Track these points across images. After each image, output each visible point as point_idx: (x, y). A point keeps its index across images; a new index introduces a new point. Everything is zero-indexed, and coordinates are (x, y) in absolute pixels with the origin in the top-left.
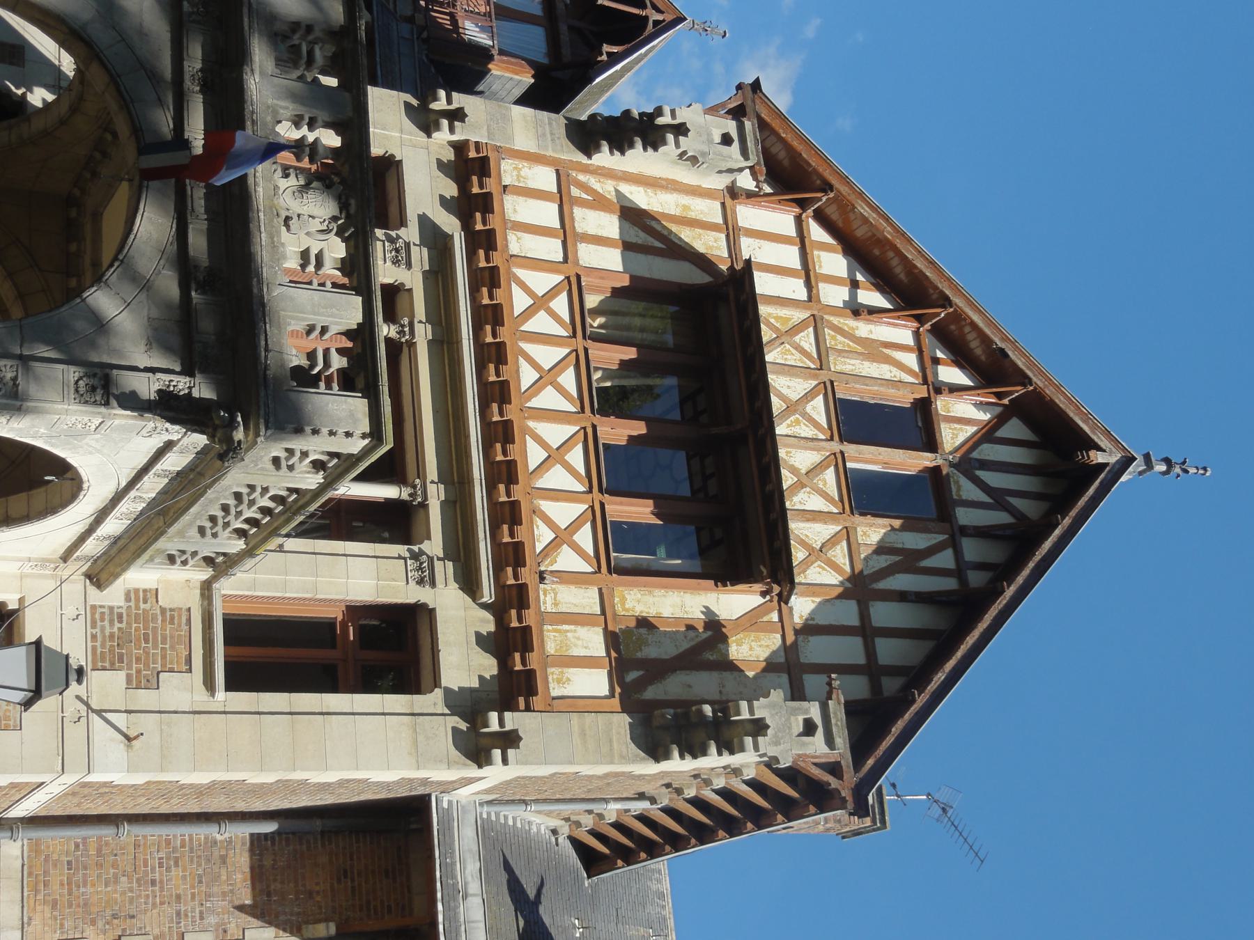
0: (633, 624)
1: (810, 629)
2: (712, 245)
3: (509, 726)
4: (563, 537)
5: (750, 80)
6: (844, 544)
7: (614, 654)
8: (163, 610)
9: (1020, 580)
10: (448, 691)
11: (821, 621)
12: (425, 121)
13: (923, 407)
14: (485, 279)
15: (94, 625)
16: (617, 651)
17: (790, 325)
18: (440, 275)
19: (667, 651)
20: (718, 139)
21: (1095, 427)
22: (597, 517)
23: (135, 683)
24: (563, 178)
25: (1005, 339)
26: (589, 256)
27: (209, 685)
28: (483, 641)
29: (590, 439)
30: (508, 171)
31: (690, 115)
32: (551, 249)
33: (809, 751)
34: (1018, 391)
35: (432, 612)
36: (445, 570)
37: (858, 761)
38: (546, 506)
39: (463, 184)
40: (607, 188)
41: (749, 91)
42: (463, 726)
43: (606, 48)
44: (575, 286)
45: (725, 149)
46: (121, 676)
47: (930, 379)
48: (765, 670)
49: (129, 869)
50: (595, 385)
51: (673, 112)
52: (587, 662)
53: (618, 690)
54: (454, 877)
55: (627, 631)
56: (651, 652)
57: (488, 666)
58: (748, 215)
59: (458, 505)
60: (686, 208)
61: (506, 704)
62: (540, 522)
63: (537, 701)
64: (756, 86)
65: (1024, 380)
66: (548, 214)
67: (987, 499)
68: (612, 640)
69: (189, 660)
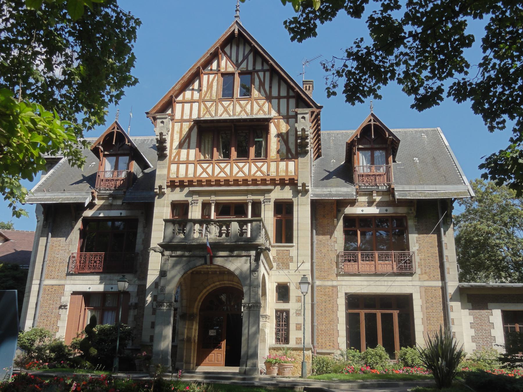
0: (278, 155)
1: (279, 112)
2: (186, 127)
4: (259, 169)
5: (146, 115)
6: (258, 101)
7: (285, 160)
8: (277, 255)
9: (268, 58)
10: (293, 197)
11: (277, 109)
12: (162, 194)
13: (223, 75)
14: (200, 183)
15: (280, 269)
16: (284, 159)
17: (205, 108)
18: (199, 193)
20: (162, 125)
21: (229, 31)
22: (254, 161)
23: (292, 261)
24: (173, 163)
25: (207, 53)
26: (192, 158)
27: (292, 246)
28: (282, 189)
29: (236, 162)
30: (173, 176)
31: (157, 132)
32: (191, 167)
33: (308, 119)
34: (220, 50)
35: (276, 199)
36: (267, 196)
37: (311, 107)
38: (253, 172)
39: (177, 186)
40: (174, 152)
42: (300, 194)
43: (127, 143)
44: (200, 162)
46: (290, 264)
47: (216, 72)
48: (288, 124)
49: (322, 260)
50: (223, 159)
51: (157, 136)
52: (287, 166)
53: (293, 160)
54: (327, 194)
55: (280, 156)
56: (284, 151)
57: (287, 188)
58: (178, 116)
59: (253, 192)
60: (177, 132)
61: (296, 184)
62: (256, 175)
63: (296, 178)
64: (147, 113)
66: (182, 167)
68: (282, 160)
69: (287, 250)
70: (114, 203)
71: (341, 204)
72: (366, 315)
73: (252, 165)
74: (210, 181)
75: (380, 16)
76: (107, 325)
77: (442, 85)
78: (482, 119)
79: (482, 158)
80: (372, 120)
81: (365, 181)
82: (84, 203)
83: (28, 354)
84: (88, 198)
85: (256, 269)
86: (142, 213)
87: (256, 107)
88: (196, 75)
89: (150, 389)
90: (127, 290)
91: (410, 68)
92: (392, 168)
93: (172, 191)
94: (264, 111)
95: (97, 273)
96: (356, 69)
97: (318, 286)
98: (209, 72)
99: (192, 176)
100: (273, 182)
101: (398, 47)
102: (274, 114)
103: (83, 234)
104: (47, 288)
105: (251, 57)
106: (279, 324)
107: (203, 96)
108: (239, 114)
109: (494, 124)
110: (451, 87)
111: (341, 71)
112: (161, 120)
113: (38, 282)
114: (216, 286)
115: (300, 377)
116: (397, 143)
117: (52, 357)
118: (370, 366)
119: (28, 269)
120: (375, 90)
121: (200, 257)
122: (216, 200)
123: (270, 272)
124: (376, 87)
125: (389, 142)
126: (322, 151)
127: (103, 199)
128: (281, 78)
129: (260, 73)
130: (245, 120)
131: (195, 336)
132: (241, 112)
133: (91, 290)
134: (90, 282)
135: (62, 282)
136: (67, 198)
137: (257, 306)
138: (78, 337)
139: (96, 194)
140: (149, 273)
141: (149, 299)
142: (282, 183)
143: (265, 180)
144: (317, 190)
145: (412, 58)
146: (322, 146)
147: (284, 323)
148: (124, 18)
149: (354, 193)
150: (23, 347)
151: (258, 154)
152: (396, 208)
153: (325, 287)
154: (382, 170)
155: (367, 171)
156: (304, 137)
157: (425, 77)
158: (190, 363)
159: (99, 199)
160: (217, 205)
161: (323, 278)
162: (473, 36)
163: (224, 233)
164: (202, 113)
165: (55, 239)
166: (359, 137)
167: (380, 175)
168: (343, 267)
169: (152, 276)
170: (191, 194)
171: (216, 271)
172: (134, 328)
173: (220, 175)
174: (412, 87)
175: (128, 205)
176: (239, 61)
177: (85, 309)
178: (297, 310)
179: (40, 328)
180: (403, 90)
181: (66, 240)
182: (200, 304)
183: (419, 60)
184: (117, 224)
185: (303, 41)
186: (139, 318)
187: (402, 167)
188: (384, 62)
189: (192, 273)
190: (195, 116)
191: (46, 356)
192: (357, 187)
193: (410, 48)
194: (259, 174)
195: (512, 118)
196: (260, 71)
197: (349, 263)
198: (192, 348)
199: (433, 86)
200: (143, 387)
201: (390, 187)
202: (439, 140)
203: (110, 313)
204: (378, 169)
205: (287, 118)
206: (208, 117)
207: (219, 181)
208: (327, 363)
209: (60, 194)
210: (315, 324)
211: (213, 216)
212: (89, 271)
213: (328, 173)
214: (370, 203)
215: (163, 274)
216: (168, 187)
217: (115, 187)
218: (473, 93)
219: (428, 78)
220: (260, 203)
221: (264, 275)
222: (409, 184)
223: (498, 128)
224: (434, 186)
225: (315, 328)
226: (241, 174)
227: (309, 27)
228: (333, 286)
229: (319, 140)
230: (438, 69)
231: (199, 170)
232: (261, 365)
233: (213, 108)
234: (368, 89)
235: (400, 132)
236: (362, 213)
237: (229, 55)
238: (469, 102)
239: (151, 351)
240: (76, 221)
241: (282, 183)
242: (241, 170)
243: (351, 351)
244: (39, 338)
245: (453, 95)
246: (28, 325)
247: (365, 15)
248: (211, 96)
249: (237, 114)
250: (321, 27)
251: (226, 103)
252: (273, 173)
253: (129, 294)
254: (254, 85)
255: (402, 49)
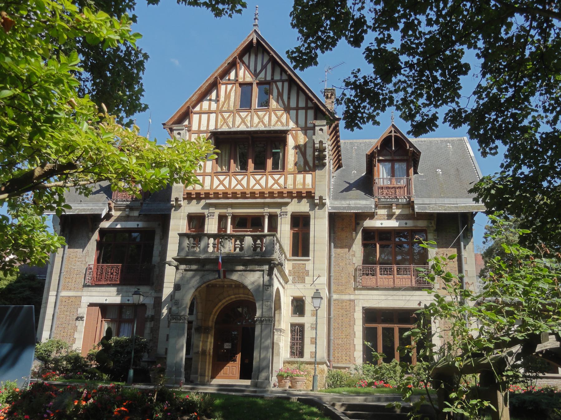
1: (297, 123)
3: (318, 198)
9: (287, 69)
11: (295, 120)
12: (178, 207)
13: (241, 85)
14: (216, 195)
18: (216, 206)
19: (302, 160)
21: (247, 40)
22: (271, 173)
23: (308, 275)
25: (225, 63)
26: (209, 169)
27: (308, 260)
28: (299, 202)
29: (253, 173)
32: (208, 179)
33: (326, 131)
34: (238, 59)
38: (269, 185)
41: (165, 126)
42: (317, 207)
44: (217, 174)
45: (182, 134)
47: (234, 82)
54: (345, 207)
55: (298, 168)
56: (302, 163)
57: (304, 201)
58: (195, 127)
59: (269, 205)
63: (313, 191)
64: (164, 124)
65: (235, 58)
67: (264, 70)
68: (300, 172)
70: (131, 214)
71: (360, 217)
72: (384, 329)
73: (270, 177)
74: (227, 193)
75: (377, 48)
76: (124, 337)
77: (437, 113)
78: (478, 144)
79: (471, 183)
80: (393, 132)
81: (385, 193)
82: (100, 215)
83: (45, 364)
84: (105, 210)
85: (270, 284)
86: (159, 225)
87: (274, 118)
88: (214, 85)
89: (154, 396)
90: (143, 303)
91: (408, 95)
92: (413, 180)
93: (189, 203)
94: (281, 123)
95: (114, 285)
96: (355, 97)
97: (335, 300)
98: (227, 82)
99: (208, 188)
100: (290, 195)
101: (396, 76)
102: (292, 125)
103: (100, 245)
104: (64, 300)
105: (269, 67)
106: (294, 338)
107: (220, 107)
108: (257, 125)
109: (488, 150)
110: (447, 114)
111: (340, 99)
112: (178, 132)
113: (55, 293)
114: (231, 299)
115: (311, 390)
116: (418, 155)
117: (69, 368)
118: (384, 381)
119: (45, 280)
120: (374, 116)
121: (214, 271)
122: (232, 213)
123: (286, 286)
124: (375, 113)
125: (410, 154)
126: (343, 161)
127: (120, 210)
128: (299, 89)
129: (278, 83)
130: (262, 132)
131: (210, 349)
132: (259, 123)
133: (107, 302)
134: (107, 294)
135: (79, 294)
136: (84, 209)
137: (269, 320)
138: (94, 349)
139: (113, 205)
140: (164, 286)
141: (165, 311)
142: (299, 196)
143: (282, 193)
144: (336, 203)
145: (410, 86)
146: (343, 157)
147: (298, 337)
148: (133, 52)
149: (373, 206)
150: (40, 358)
151: (275, 166)
152: (415, 221)
153: (343, 301)
154: (403, 183)
155: (387, 183)
156: (321, 149)
157: (422, 104)
158: (205, 376)
159: (116, 210)
160: (234, 217)
161: (341, 292)
162: (468, 65)
163: (238, 247)
164: (219, 124)
165: (72, 250)
166: (379, 149)
167: (400, 188)
168: (360, 281)
169: (168, 290)
170: (208, 206)
171: (232, 285)
172: (150, 340)
173: (236, 188)
174: (410, 113)
175: (144, 217)
176: (258, 71)
177: (102, 321)
178: (312, 324)
179: (56, 340)
180: (401, 117)
181: (83, 251)
182: (216, 317)
183: (415, 88)
184: (135, 235)
185: (305, 69)
186: (155, 331)
187: (424, 179)
188: (382, 90)
189: (207, 286)
190: (212, 128)
191: (63, 368)
192: (376, 200)
193: (407, 77)
194: (276, 187)
195: (505, 143)
196: (278, 81)
197: (367, 277)
198: (207, 361)
199: (428, 113)
200: (148, 395)
201: (410, 200)
202: (465, 150)
203: (127, 325)
204: (398, 181)
205: (306, 130)
206: (225, 129)
207: (236, 193)
208: (342, 377)
209: (77, 205)
210: (332, 338)
211: (229, 230)
212: (106, 283)
213: (348, 185)
214: (390, 216)
215: (177, 287)
216: (184, 199)
217: (132, 198)
218: (468, 118)
219: (425, 105)
220: (277, 216)
221: (278, 289)
222: (429, 197)
223: (491, 154)
224: (455, 200)
225: (332, 342)
226: (257, 187)
227: (311, 56)
228: (350, 300)
229: (339, 151)
230: (434, 97)
231: (216, 182)
232: (274, 380)
233: (231, 119)
234: (367, 116)
235: (425, 141)
236: (381, 226)
237: (247, 64)
238: (466, 127)
239: (165, 364)
240: (93, 232)
241: (299, 196)
242: (258, 182)
243: (366, 366)
244: (55, 349)
245: (449, 121)
246: (45, 336)
247: (364, 45)
248: (229, 106)
249: (255, 125)
250: (321, 57)
251: (243, 114)
252: (290, 186)
253: (146, 306)
254: (272, 95)
255: (399, 77)
